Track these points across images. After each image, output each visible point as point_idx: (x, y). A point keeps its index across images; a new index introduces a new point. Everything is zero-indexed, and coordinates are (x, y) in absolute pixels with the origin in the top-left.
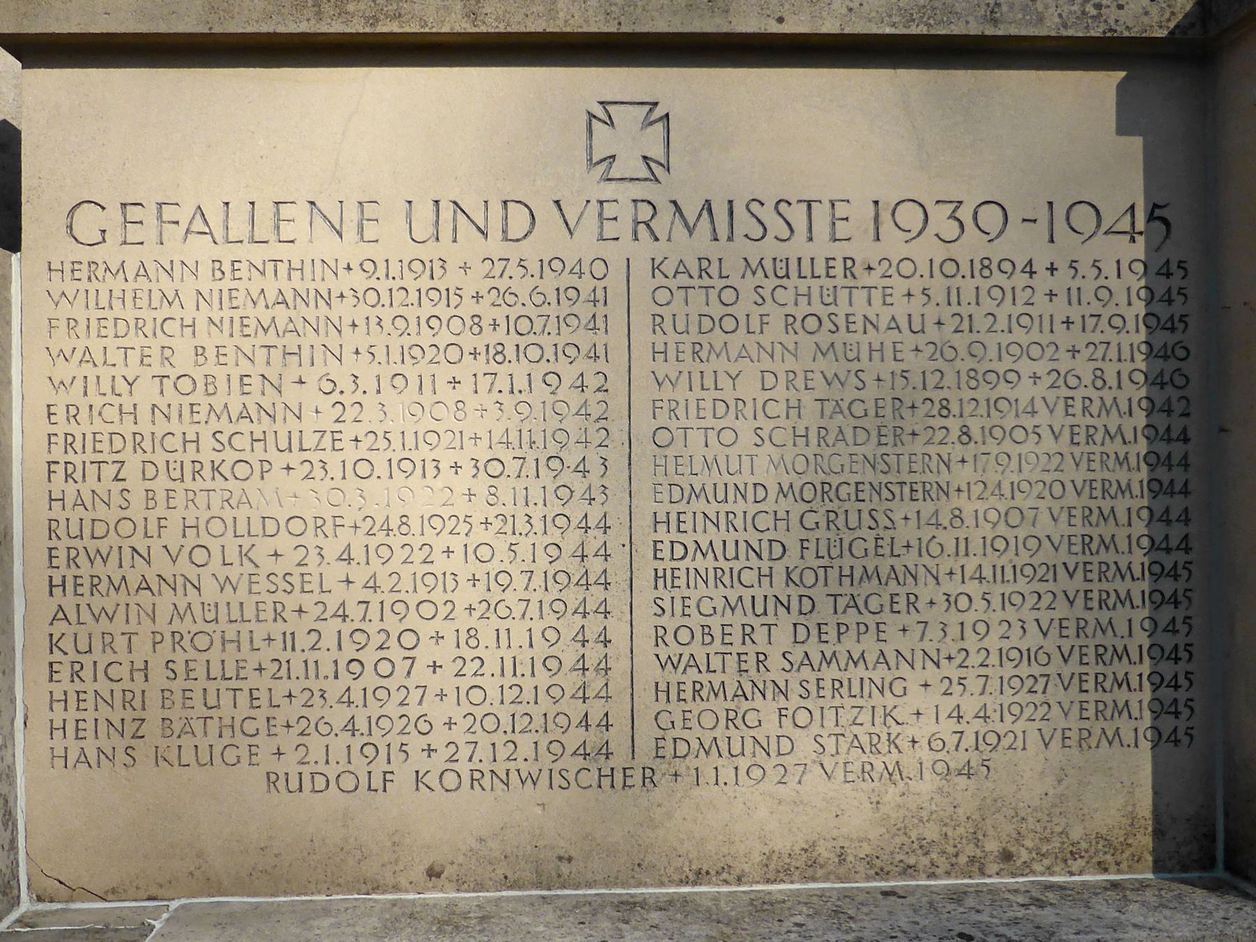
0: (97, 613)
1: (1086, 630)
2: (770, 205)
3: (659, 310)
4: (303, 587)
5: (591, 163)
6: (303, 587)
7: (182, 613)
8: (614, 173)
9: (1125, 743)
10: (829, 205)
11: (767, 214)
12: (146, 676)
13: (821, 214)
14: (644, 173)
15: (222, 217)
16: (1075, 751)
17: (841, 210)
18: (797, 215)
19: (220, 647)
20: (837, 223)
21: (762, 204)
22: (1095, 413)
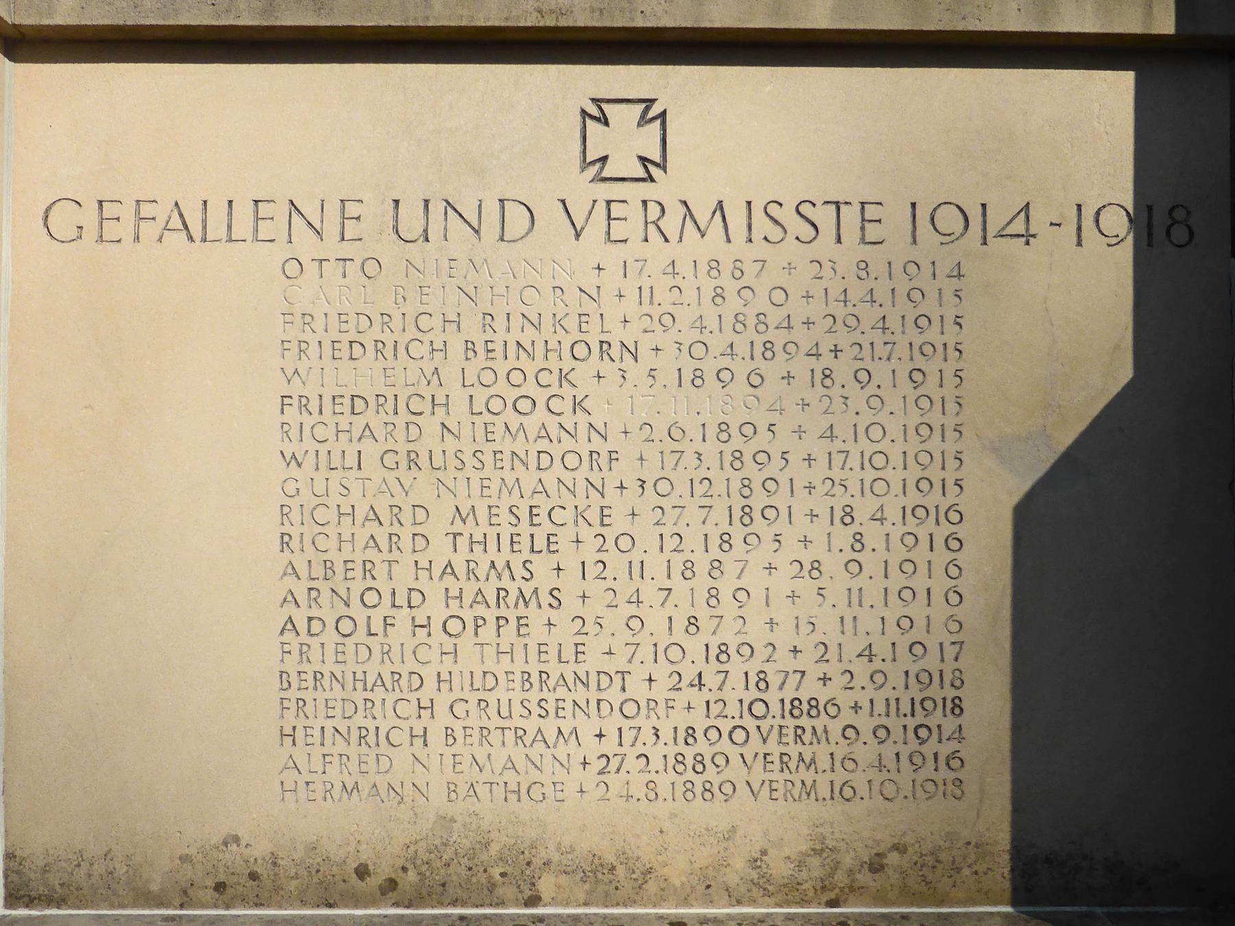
0: (641, 173)
1: (401, 682)
2: (789, 208)
3: (287, 501)
4: (602, 521)
5: (585, 164)
6: (602, 521)
7: (464, 516)
8: (606, 173)
9: (820, 797)
10: (859, 207)
11: (786, 215)
12: (425, 741)
13: (850, 215)
14: (641, 173)
15: (199, 215)
16: (781, 802)
17: (871, 212)
18: (824, 217)
19: (298, 657)
20: (867, 225)
21: (781, 205)
22: (482, 577)
